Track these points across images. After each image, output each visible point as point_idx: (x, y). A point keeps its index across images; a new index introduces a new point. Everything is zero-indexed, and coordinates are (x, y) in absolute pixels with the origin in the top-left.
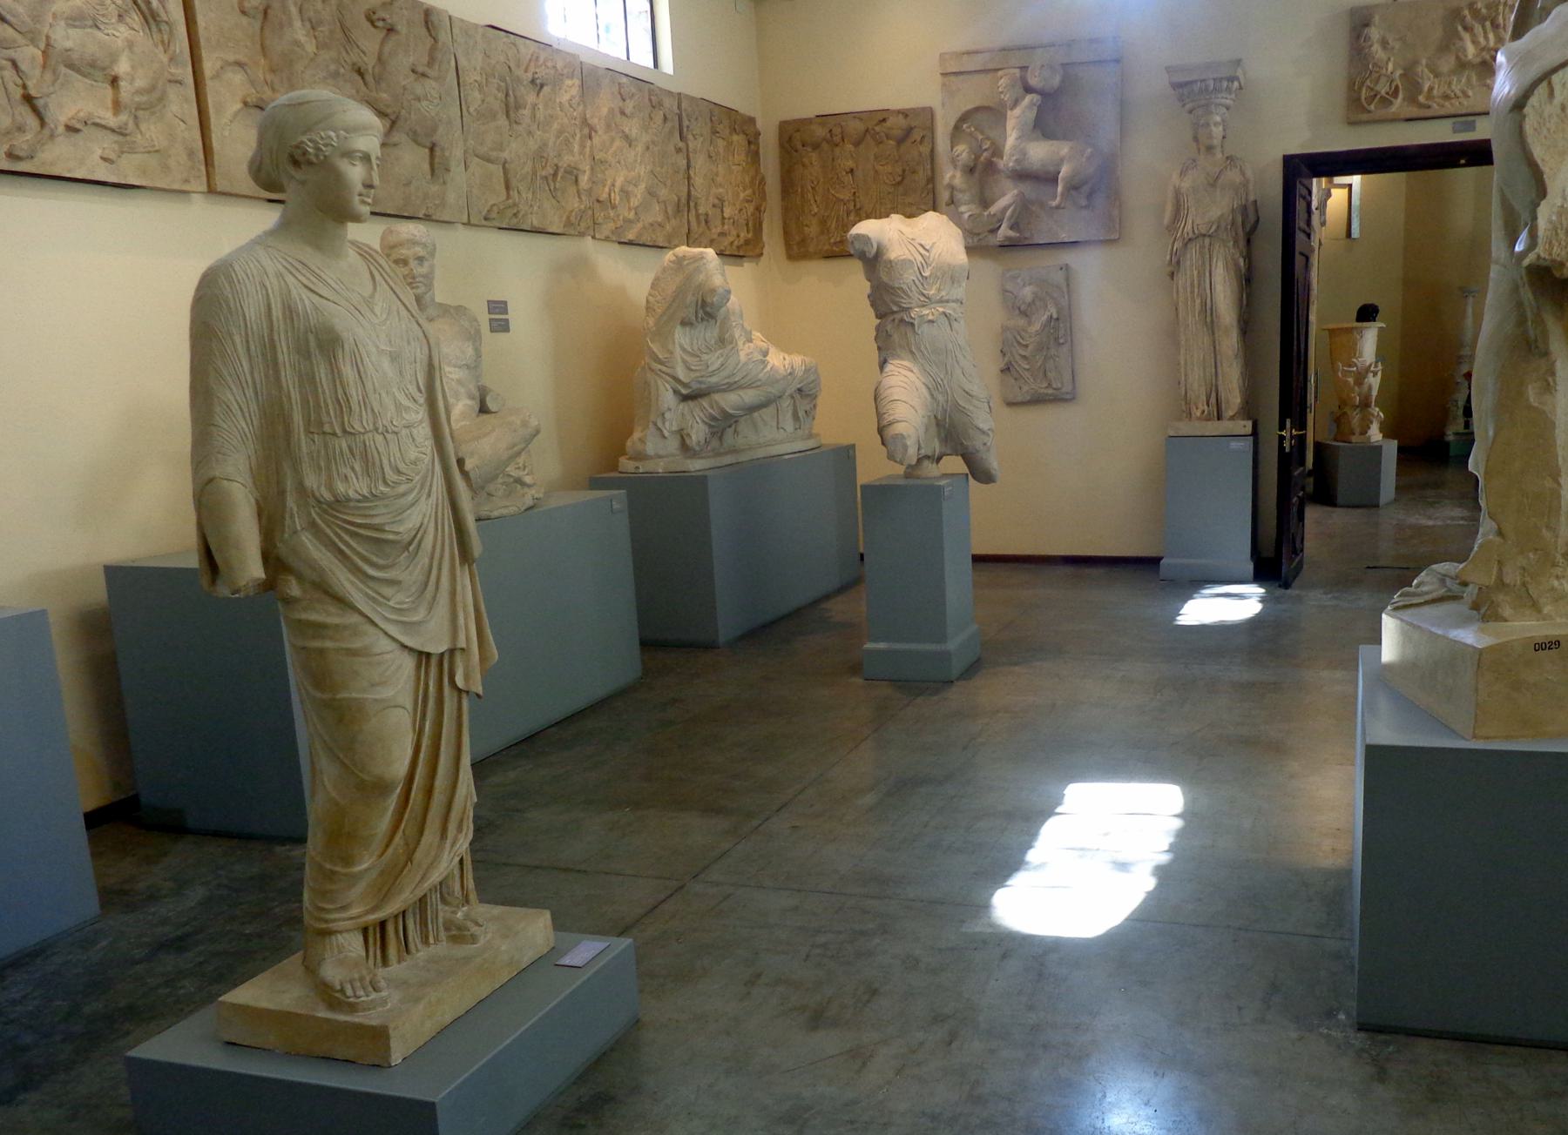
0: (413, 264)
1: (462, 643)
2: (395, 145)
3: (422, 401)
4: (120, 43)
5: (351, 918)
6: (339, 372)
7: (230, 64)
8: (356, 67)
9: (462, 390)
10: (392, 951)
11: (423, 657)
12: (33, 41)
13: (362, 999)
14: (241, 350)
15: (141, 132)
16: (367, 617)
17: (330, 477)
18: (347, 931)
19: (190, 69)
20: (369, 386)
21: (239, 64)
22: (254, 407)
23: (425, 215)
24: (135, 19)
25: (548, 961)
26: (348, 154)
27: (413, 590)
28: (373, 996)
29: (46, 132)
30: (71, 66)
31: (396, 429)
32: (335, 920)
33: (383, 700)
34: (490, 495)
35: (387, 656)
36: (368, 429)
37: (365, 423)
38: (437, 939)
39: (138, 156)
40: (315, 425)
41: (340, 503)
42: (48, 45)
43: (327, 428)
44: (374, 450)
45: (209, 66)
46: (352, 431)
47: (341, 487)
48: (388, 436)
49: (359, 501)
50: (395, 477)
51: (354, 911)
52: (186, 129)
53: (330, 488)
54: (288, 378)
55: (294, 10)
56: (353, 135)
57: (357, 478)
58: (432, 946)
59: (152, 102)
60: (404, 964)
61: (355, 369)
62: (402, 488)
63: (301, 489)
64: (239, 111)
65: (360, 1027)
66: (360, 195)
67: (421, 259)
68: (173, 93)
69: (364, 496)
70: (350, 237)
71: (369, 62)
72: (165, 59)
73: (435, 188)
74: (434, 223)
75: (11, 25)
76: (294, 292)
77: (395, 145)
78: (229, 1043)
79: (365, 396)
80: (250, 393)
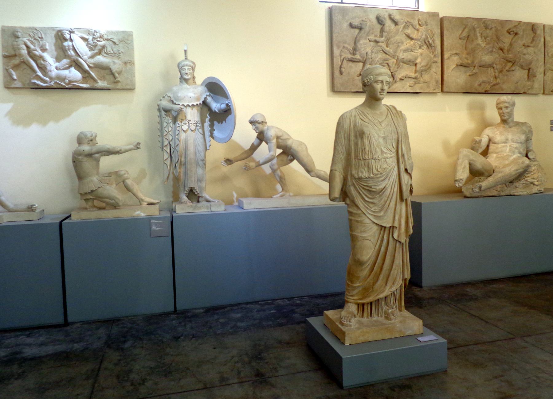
0: (503, 109)
1: (396, 224)
2: (513, 71)
3: (394, 151)
4: (419, 54)
5: (354, 300)
6: (363, 141)
7: (453, 54)
8: (500, 48)
9: (517, 151)
10: (365, 314)
11: (382, 228)
12: (394, 58)
13: (345, 323)
14: (343, 136)
15: (422, 78)
16: (363, 212)
17: (358, 171)
18: (352, 303)
19: (440, 58)
20: (372, 146)
21: (456, 54)
22: (345, 151)
23: (523, 92)
24: (425, 47)
25: (414, 336)
26: (377, 82)
27: (380, 207)
28: (348, 323)
29: (394, 81)
30: (404, 62)
31: (380, 159)
32: (349, 299)
33: (363, 237)
34: (516, 187)
35: (367, 225)
36: (370, 158)
37: (369, 157)
38: (381, 316)
39: (421, 85)
40: (356, 157)
41: (360, 179)
42: (398, 58)
43: (359, 158)
44: (371, 164)
45: (446, 56)
46: (365, 158)
47: (360, 174)
48: (376, 161)
49: (365, 179)
50: (377, 172)
51: (356, 298)
52: (436, 75)
53: (358, 175)
54: (352, 143)
55: (478, 35)
56: (377, 76)
57: (365, 172)
58: (379, 317)
59: (427, 68)
60: (368, 319)
61: (369, 141)
62: (379, 176)
63: (352, 175)
64: (455, 67)
65: (341, 330)
66: (380, 92)
67: (507, 107)
68: (434, 65)
69: (366, 177)
70: (383, 103)
71: (506, 46)
72: (432, 56)
73: (529, 83)
74: (546, 95)
75: (388, 55)
76: (357, 120)
77: (513, 71)
78: (325, 324)
79: (371, 149)
80: (344, 148)
